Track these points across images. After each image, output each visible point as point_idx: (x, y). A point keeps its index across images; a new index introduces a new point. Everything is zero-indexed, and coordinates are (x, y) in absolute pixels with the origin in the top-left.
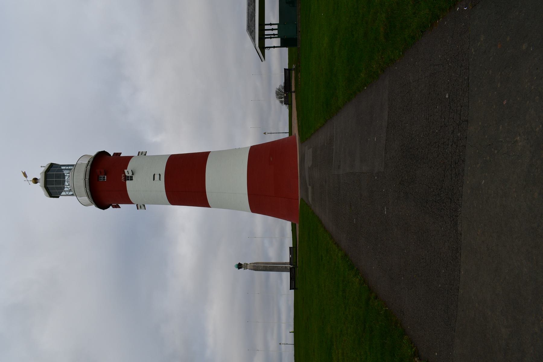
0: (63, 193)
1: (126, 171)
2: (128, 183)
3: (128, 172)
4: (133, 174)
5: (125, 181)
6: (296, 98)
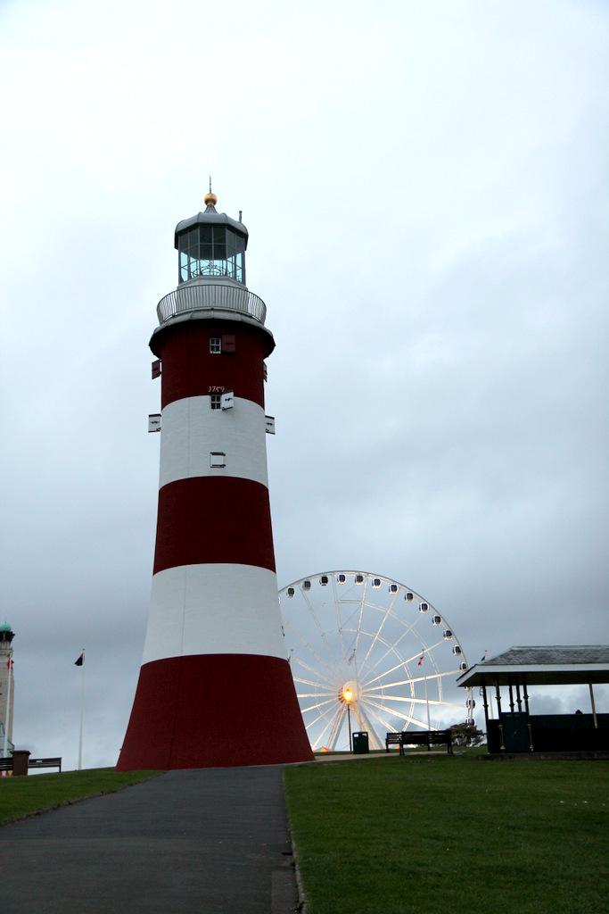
0: (184, 256)
1: (231, 395)
2: (207, 399)
3: (228, 399)
4: (224, 409)
5: (209, 394)
6: (381, 758)
